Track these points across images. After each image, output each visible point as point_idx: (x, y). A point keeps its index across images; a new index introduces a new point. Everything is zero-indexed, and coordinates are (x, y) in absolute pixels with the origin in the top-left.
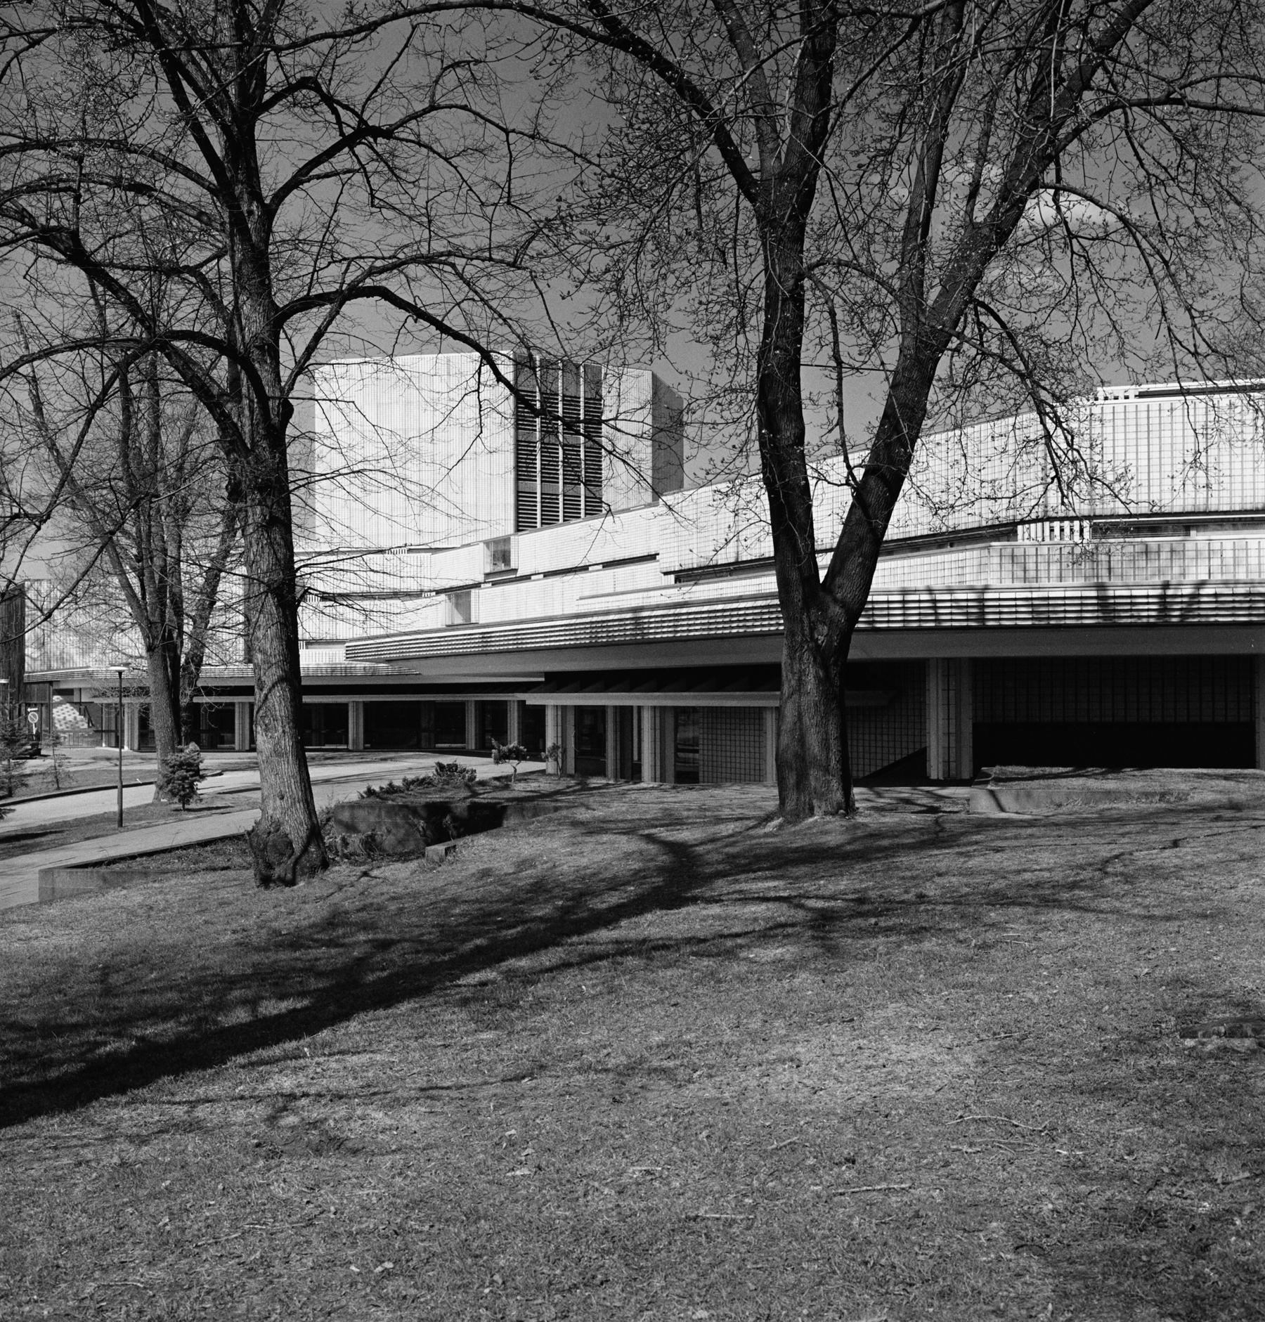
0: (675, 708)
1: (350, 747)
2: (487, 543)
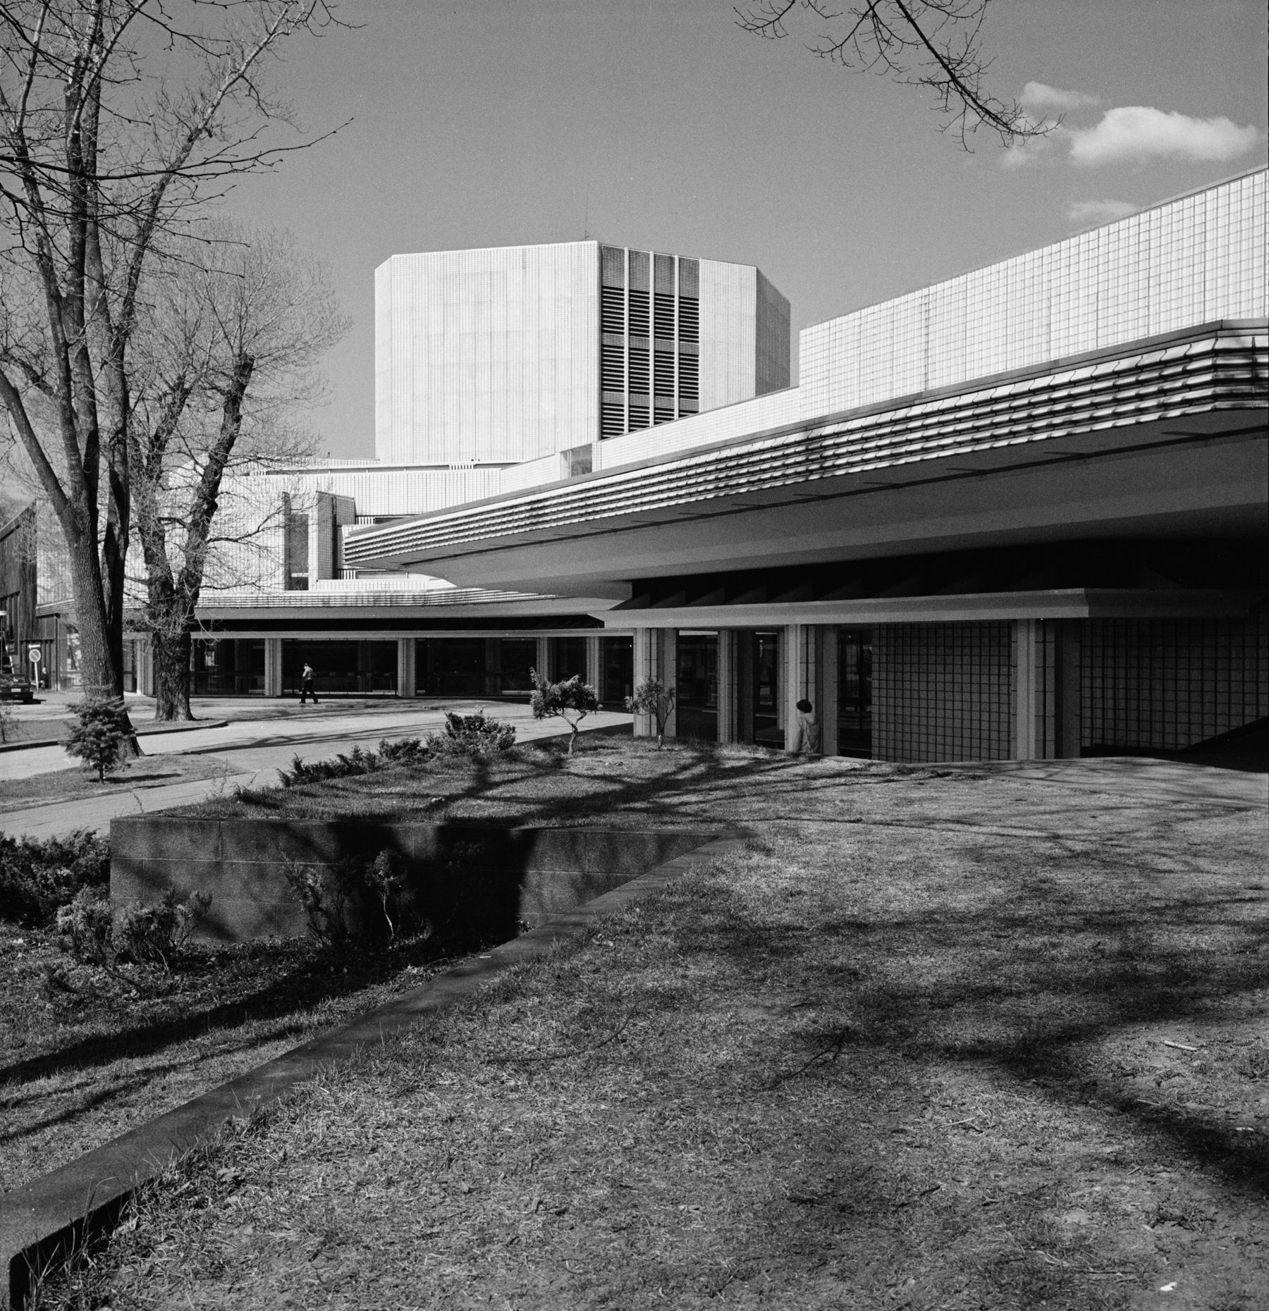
0: (838, 628)
1: (400, 693)
2: (564, 453)
